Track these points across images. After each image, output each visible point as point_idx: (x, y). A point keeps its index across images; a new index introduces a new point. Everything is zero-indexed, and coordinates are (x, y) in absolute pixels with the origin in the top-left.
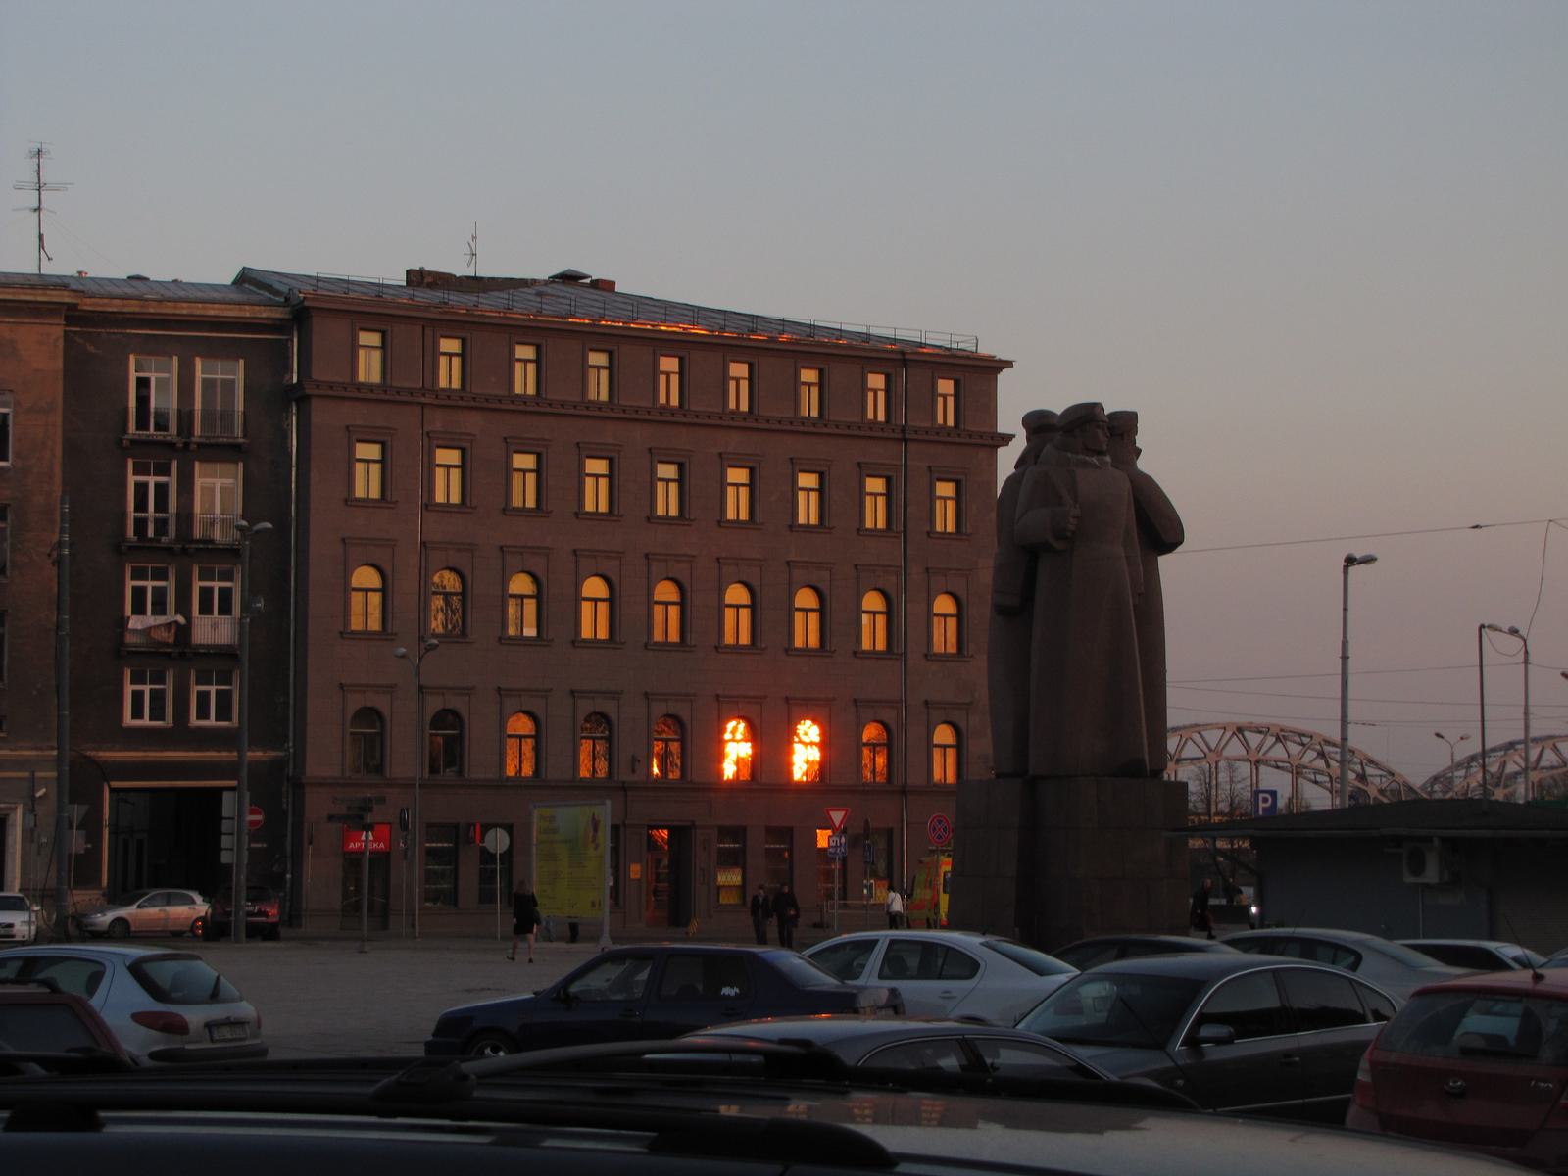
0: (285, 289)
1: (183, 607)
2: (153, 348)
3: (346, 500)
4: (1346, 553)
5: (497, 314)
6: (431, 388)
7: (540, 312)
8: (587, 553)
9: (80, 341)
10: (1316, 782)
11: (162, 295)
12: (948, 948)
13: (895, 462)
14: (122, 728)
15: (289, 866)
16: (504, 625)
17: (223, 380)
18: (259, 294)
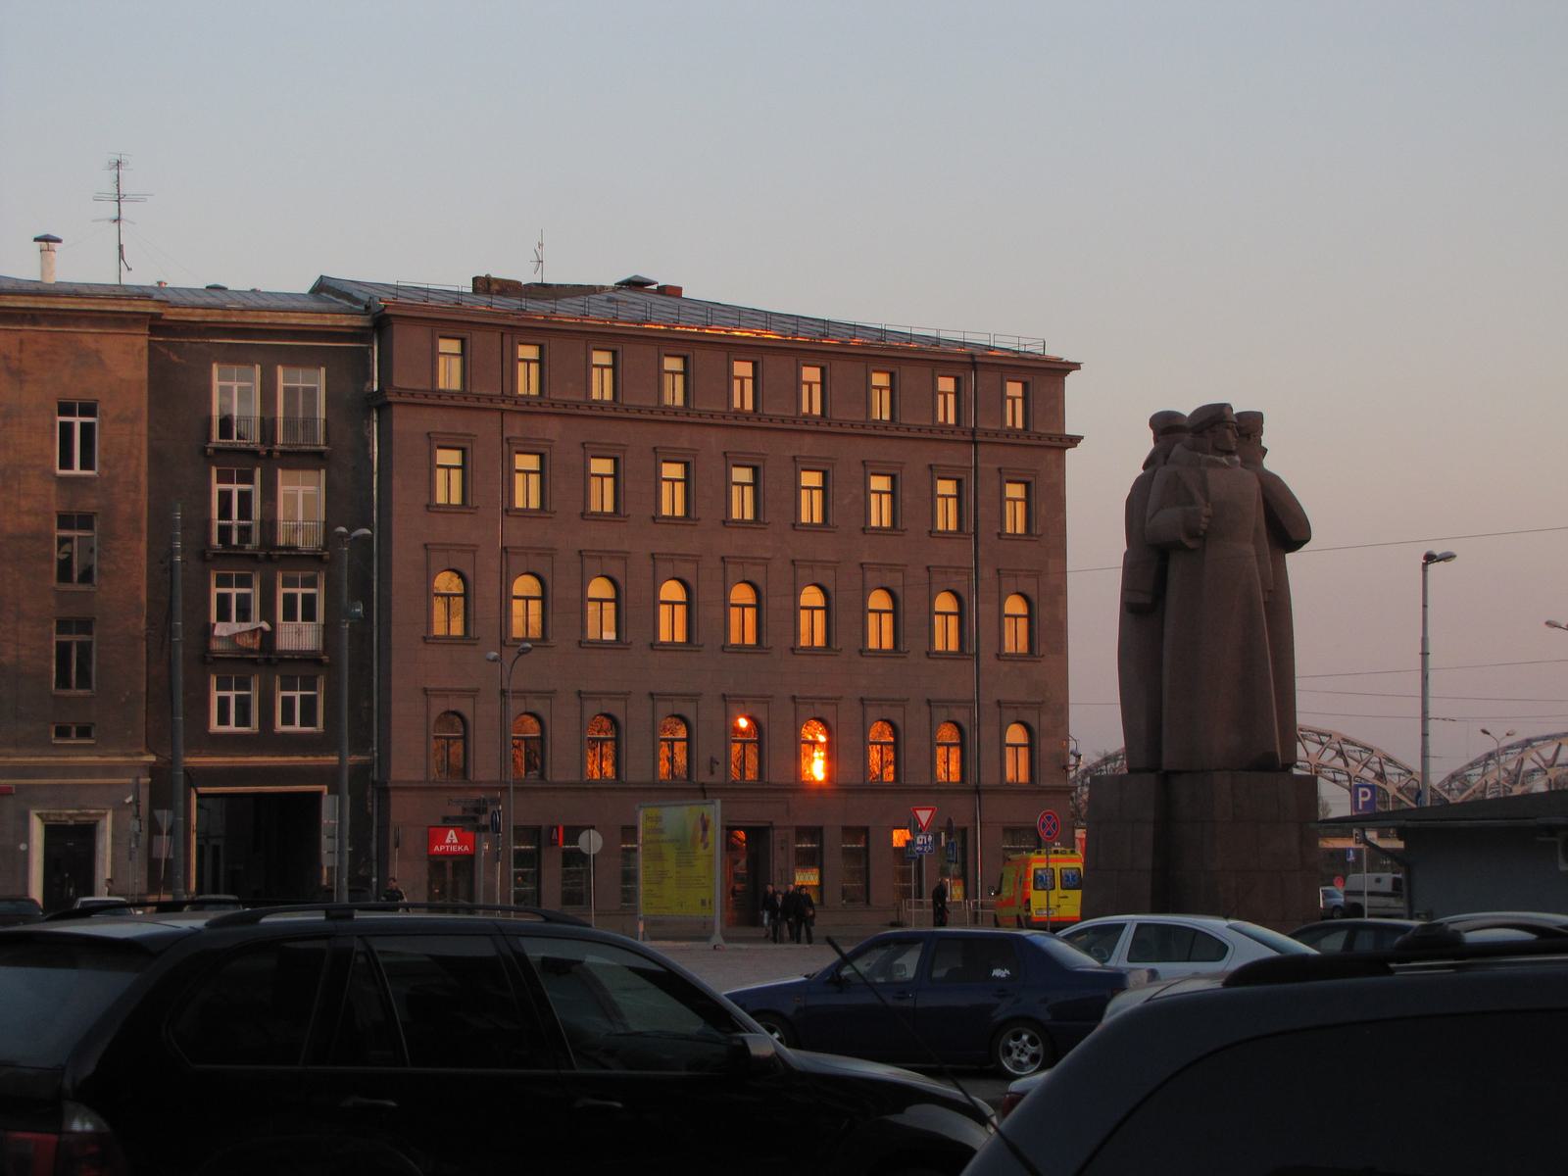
0: (366, 298)
1: (268, 613)
2: (235, 357)
3: (428, 506)
4: (1423, 554)
5: (574, 321)
6: (509, 394)
7: (615, 318)
8: (875, 566)
9: (164, 350)
10: (1335, 781)
11: (244, 304)
12: (1196, 931)
13: (966, 464)
14: (209, 734)
15: (375, 871)
16: (796, 634)
17: (305, 389)
18: (337, 302)
